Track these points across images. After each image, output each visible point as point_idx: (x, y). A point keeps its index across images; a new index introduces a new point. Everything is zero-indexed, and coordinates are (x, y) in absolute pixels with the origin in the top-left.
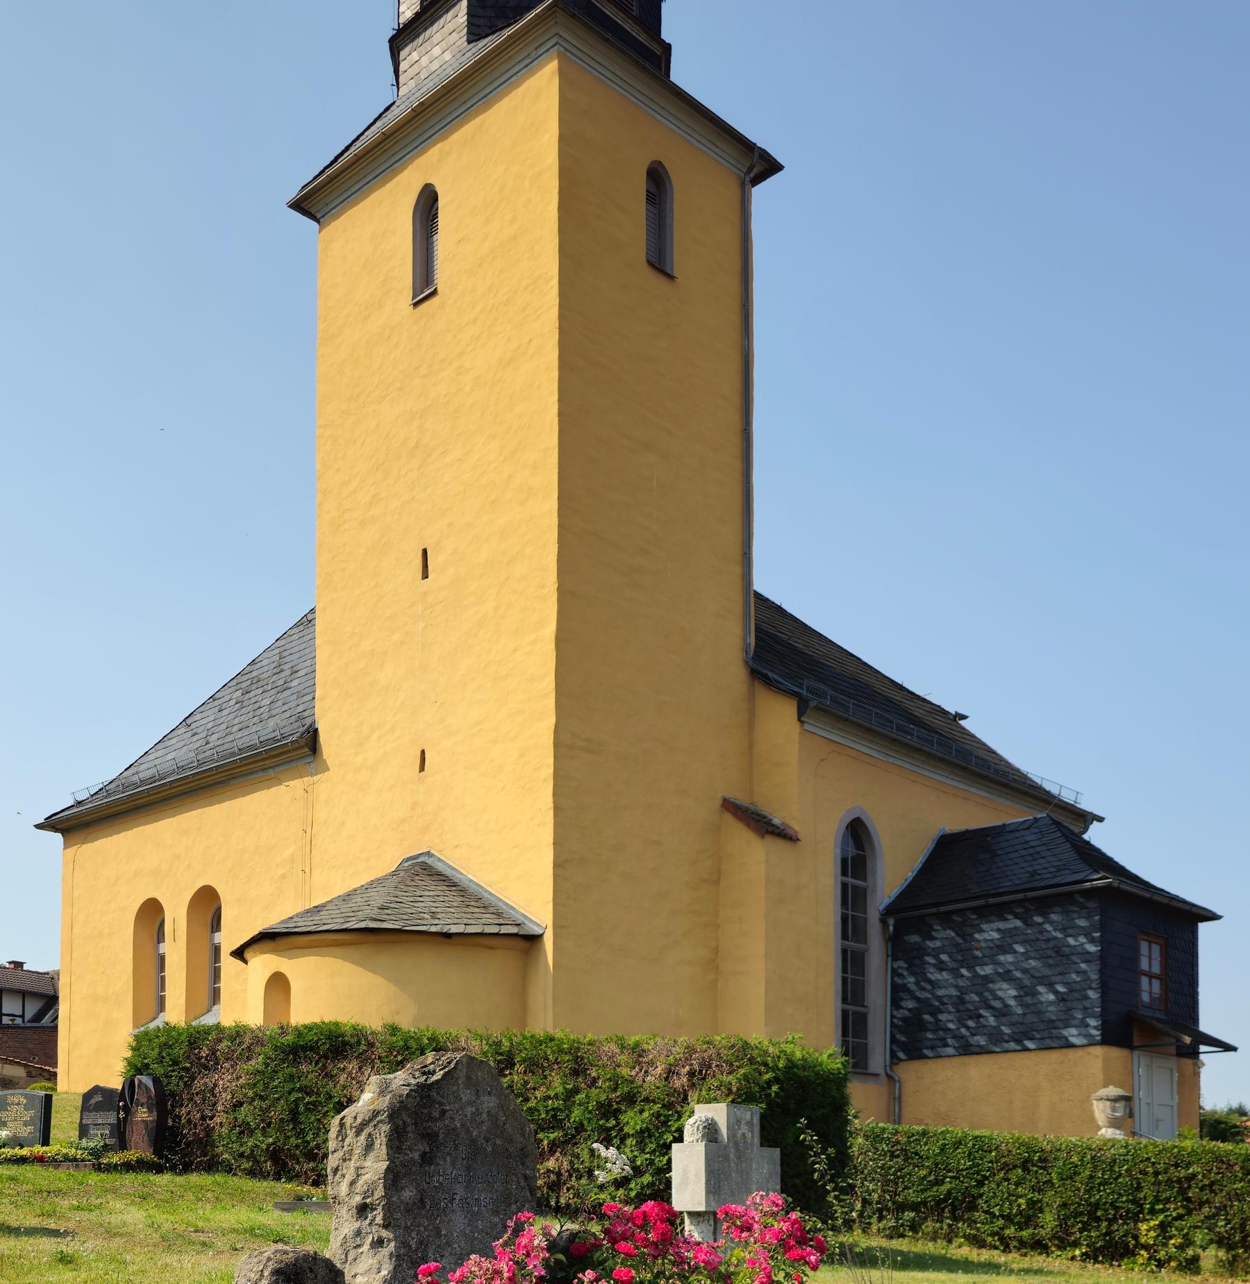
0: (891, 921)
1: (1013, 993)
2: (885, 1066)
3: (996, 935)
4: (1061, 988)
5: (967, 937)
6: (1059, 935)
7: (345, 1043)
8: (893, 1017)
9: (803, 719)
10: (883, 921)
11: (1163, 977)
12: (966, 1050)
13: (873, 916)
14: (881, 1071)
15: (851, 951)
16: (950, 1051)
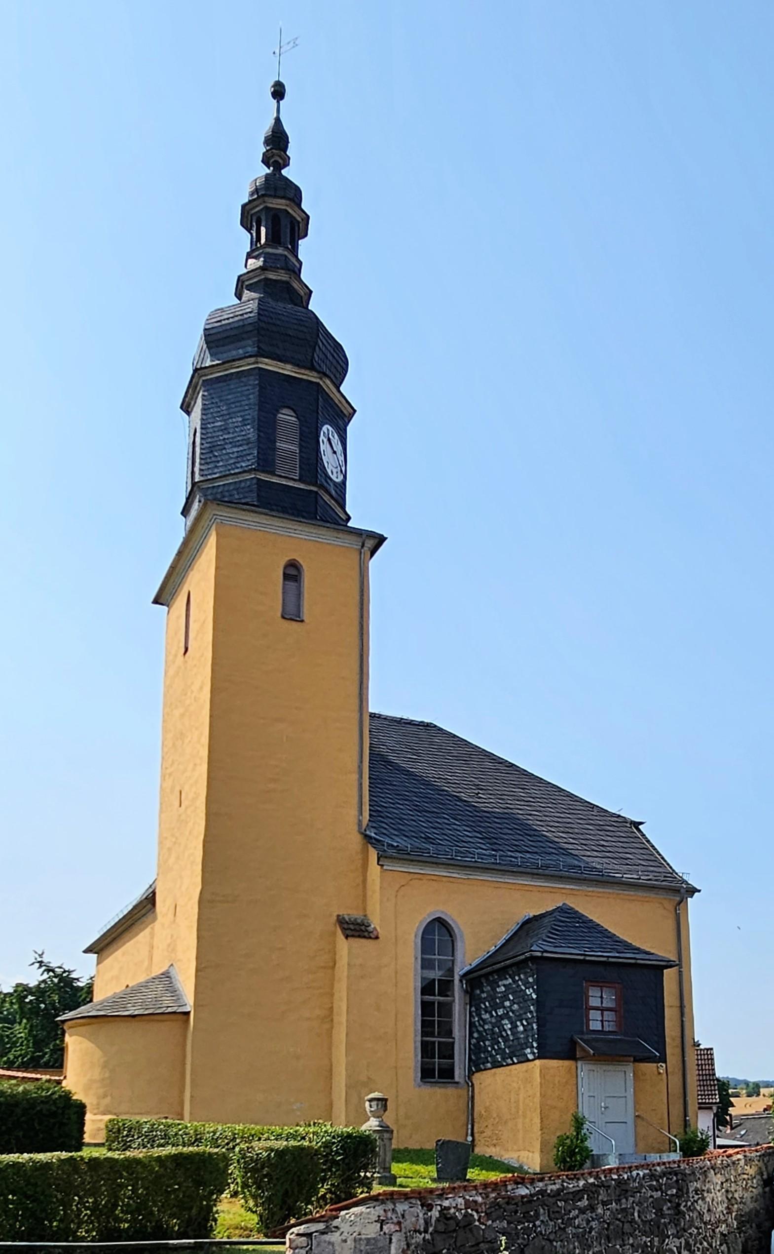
0: (464, 982)
1: (509, 1026)
2: (465, 1076)
3: (503, 989)
4: (525, 1023)
5: (482, 1204)
6: (523, 988)
7: (479, 1070)
8: (470, 1043)
9: (380, 863)
10: (461, 981)
11: (618, 1009)
12: (497, 1065)
13: (457, 978)
14: (462, 1081)
15: (438, 1003)
16: (489, 1065)
